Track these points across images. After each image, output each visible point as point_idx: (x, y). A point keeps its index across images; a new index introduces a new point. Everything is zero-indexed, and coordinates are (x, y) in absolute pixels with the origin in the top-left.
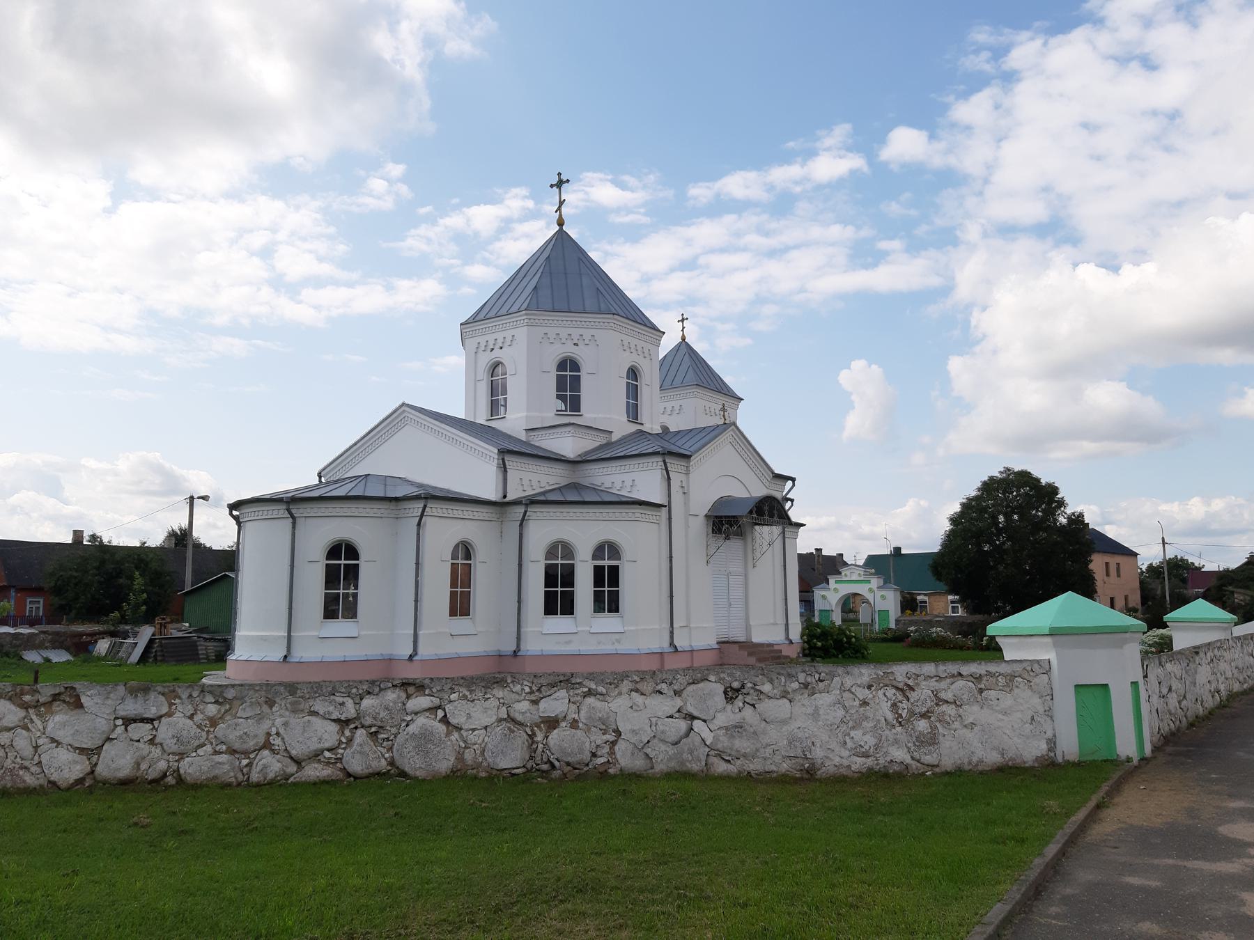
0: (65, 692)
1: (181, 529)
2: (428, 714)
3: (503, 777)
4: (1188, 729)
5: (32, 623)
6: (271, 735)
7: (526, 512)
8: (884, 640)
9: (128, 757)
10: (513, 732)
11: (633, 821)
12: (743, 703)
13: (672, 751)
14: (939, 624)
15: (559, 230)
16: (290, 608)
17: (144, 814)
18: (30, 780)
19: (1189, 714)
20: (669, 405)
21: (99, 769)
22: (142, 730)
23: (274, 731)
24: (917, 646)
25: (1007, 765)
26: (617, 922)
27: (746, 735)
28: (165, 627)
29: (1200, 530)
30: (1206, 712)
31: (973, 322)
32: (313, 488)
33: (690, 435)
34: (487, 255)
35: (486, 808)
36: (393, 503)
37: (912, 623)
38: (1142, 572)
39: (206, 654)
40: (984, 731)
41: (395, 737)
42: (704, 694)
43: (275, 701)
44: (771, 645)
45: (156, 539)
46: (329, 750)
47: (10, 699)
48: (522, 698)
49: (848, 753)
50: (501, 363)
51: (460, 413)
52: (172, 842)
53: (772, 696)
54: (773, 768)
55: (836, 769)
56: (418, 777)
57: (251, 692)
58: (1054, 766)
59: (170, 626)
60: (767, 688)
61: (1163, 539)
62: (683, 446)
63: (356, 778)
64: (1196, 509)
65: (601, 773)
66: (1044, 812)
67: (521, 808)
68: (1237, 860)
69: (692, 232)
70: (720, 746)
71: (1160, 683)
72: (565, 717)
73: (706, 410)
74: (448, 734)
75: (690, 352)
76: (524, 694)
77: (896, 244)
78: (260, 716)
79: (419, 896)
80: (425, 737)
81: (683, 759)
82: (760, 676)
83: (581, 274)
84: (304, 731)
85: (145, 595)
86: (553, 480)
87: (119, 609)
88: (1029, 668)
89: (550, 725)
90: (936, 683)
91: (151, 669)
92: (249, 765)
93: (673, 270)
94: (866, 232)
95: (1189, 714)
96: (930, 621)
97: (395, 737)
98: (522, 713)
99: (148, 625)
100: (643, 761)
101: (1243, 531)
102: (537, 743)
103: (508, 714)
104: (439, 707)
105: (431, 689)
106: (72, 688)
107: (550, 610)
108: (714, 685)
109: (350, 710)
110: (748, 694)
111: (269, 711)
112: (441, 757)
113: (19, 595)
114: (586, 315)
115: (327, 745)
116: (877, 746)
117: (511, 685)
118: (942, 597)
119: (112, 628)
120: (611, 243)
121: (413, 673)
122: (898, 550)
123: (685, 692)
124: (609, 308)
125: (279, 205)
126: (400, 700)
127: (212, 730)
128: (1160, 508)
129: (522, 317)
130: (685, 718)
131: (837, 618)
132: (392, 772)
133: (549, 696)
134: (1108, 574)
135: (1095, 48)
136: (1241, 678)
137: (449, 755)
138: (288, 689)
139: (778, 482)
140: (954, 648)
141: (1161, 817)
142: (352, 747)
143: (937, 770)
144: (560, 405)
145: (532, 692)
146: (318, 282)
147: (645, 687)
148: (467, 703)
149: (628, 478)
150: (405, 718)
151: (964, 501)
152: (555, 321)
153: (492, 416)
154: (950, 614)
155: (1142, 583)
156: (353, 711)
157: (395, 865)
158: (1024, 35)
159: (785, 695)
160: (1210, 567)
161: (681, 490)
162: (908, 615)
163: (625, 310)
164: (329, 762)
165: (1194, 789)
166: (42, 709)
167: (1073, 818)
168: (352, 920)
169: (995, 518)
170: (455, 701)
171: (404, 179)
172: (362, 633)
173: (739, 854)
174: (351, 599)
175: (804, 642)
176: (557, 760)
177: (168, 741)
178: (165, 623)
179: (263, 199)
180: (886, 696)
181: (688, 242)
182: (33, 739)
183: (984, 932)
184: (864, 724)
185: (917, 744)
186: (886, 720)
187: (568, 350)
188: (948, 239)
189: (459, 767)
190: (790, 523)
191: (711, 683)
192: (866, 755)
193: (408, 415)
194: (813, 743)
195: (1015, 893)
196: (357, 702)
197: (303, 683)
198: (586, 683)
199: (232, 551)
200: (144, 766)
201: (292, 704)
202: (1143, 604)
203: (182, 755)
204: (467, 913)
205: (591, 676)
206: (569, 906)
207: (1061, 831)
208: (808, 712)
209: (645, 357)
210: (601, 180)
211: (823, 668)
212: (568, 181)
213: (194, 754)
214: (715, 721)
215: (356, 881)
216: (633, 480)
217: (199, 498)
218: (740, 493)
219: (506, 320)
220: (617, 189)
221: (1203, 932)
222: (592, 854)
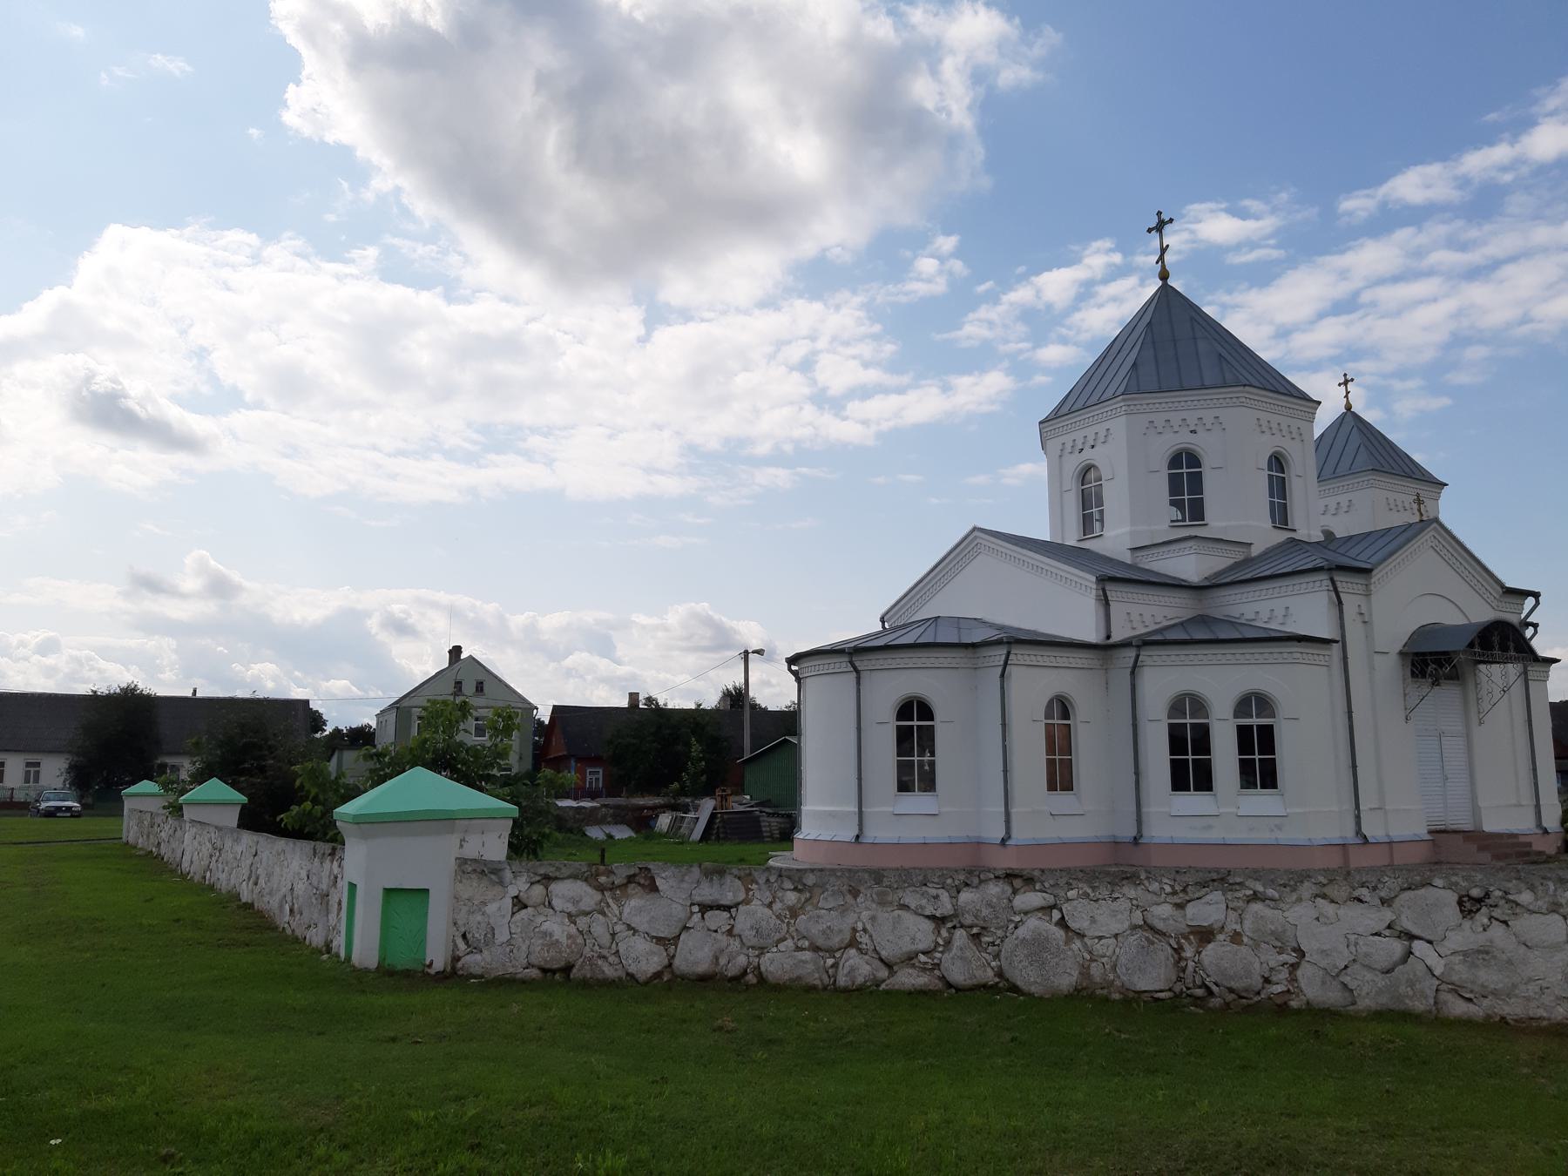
0: (640, 873)
1: (735, 688)
2: (1040, 915)
5: (593, 795)
6: (857, 931)
7: (1138, 657)
9: (706, 950)
10: (1153, 943)
12: (1490, 919)
16: (860, 779)
17: (728, 1016)
18: (609, 972)
20: (1332, 502)
21: (677, 962)
22: (718, 919)
23: (860, 926)
28: (726, 800)
32: (876, 635)
33: (1386, 539)
34: (1064, 331)
36: (970, 650)
39: (770, 832)
41: (1002, 941)
42: (1427, 905)
43: (859, 891)
45: (711, 700)
46: (923, 953)
47: (586, 880)
48: (1162, 900)
50: (1093, 466)
51: (1044, 535)
52: (760, 1053)
53: (1536, 909)
54: (1542, 1013)
57: (832, 879)
59: (731, 799)
60: (1525, 897)
63: (958, 990)
65: (1279, 1006)
69: (1348, 259)
70: (1455, 978)
74: (1068, 942)
75: (1361, 426)
76: (1164, 895)
78: (843, 908)
79: (1055, 1148)
80: (1038, 945)
82: (1514, 881)
83: (1195, 338)
84: (894, 928)
85: (703, 763)
86: (1171, 613)
87: (679, 779)
91: (715, 849)
92: (835, 966)
93: (1321, 316)
97: (1002, 941)
98: (1163, 919)
99: (708, 798)
100: (1340, 994)
102: (1186, 960)
105: (1042, 882)
106: (647, 869)
108: (1442, 892)
109: (945, 906)
110: (1496, 906)
111: (853, 902)
113: (579, 765)
114: (1184, 393)
115: (921, 946)
117: (1146, 882)
119: (673, 801)
120: (1230, 292)
125: (817, 306)
126: (1004, 896)
127: (793, 921)
129: (1118, 404)
130: (1399, 937)
132: (1001, 985)
133: (1198, 899)
138: (873, 876)
139: (1515, 599)
142: (950, 950)
144: (1175, 513)
145: (1174, 893)
147: (1336, 892)
152: (1189, 402)
153: (1084, 535)
156: (949, 906)
163: (1262, 380)
166: (618, 892)
168: (977, 1168)
171: (958, 253)
174: (927, 768)
177: (747, 933)
178: (726, 795)
179: (800, 304)
181: (1343, 274)
182: (610, 925)
187: (1183, 440)
189: (1084, 984)
193: (981, 541)
196: (953, 895)
198: (1249, 883)
199: (790, 711)
200: (723, 961)
203: (762, 950)
205: (1256, 875)
210: (1212, 211)
212: (1171, 220)
213: (775, 949)
214: (1446, 943)
217: (753, 652)
218: (1452, 618)
219: (1097, 410)
220: (1235, 219)
222: (1282, 1114)
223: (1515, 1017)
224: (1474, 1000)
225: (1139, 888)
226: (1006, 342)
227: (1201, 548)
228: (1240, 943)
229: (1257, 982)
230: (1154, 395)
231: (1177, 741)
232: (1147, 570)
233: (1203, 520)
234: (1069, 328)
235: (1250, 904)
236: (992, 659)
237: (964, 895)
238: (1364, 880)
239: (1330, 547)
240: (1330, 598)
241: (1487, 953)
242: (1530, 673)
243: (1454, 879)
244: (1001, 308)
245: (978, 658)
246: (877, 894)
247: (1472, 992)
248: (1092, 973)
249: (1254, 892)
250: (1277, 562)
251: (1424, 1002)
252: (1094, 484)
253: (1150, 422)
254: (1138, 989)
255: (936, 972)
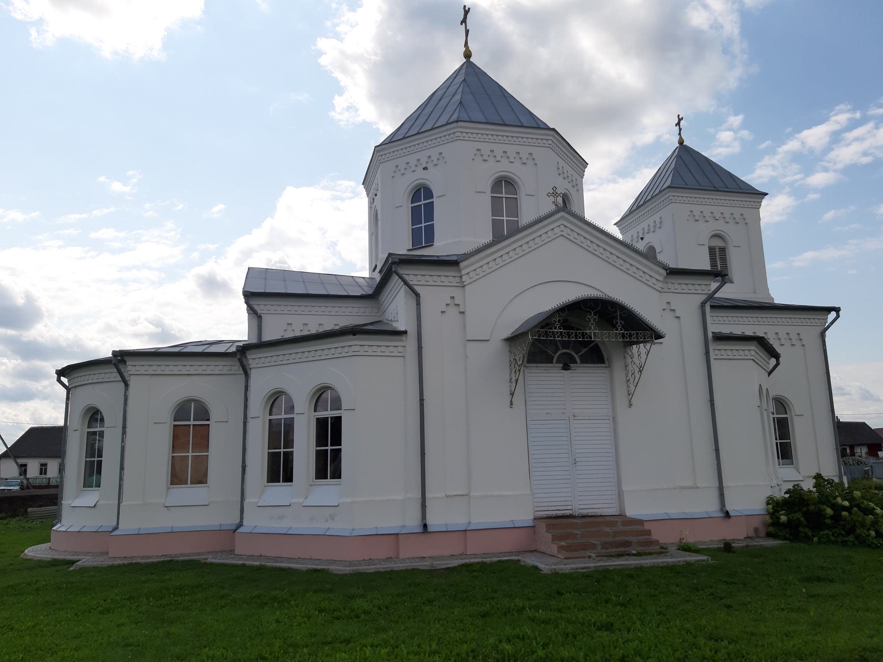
107: (321, 474)
226: (785, 176)
234: (829, 162)
244: (778, 157)
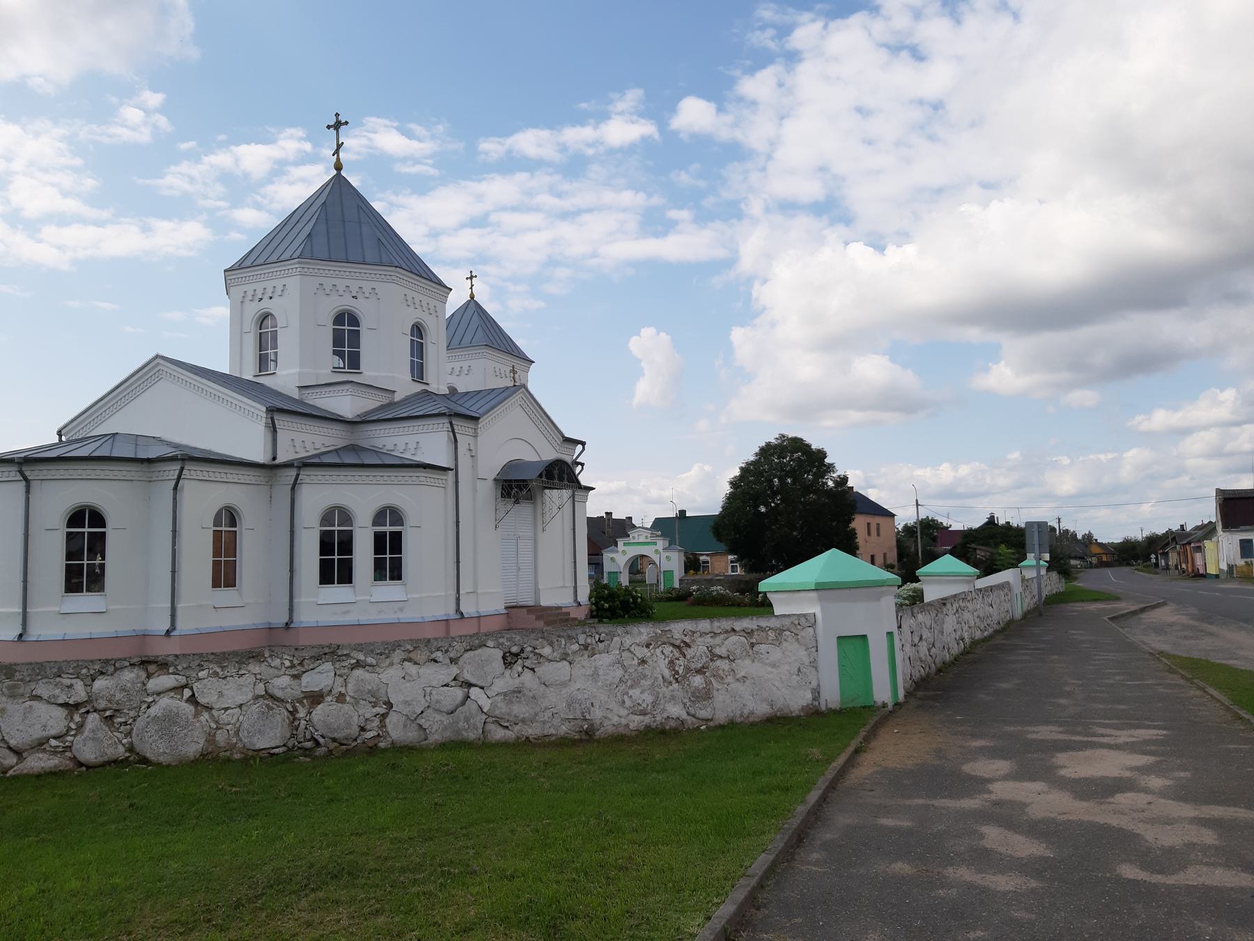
2: (172, 694)
3: (260, 758)
4: (936, 674)
7: (298, 475)
8: (669, 599)
10: (272, 709)
11: (401, 796)
12: (523, 668)
13: (446, 720)
14: (719, 582)
15: (337, 174)
16: (25, 581)
19: (938, 660)
20: (457, 366)
24: (699, 604)
25: (776, 715)
26: (372, 908)
27: (525, 700)
29: (947, 493)
30: (952, 658)
31: (755, 294)
32: (51, 447)
33: (491, 396)
35: (236, 793)
36: (145, 466)
37: (694, 582)
38: (899, 532)
40: (754, 684)
42: (482, 661)
44: (560, 608)
46: (55, 738)
48: (282, 673)
49: (626, 712)
50: (271, 315)
51: (226, 370)
54: (552, 731)
55: (615, 728)
56: (162, 763)
58: (818, 714)
60: (547, 651)
61: (917, 500)
62: (471, 408)
63: (88, 767)
64: (945, 474)
65: (371, 748)
66: (808, 759)
67: (277, 791)
68: (978, 796)
69: (482, 187)
70: (497, 713)
71: (912, 633)
72: (331, 691)
73: (495, 372)
74: (197, 715)
75: (479, 311)
76: (284, 669)
77: (684, 214)
80: (170, 719)
81: (459, 729)
82: (540, 640)
84: (25, 718)
86: (328, 441)
88: (796, 622)
89: (313, 700)
90: (710, 640)
93: (463, 226)
94: (656, 201)
95: (938, 660)
96: (711, 580)
97: (134, 720)
98: (282, 689)
100: (416, 733)
101: (985, 494)
103: (265, 690)
104: (185, 686)
105: (176, 666)
107: (326, 577)
108: (492, 650)
109: (79, 692)
110: (527, 658)
112: (188, 740)
115: (53, 732)
116: (654, 704)
117: (269, 659)
118: (723, 557)
120: (396, 193)
121: (163, 650)
122: (683, 512)
123: (461, 659)
124: (391, 260)
125: (14, 130)
126: (139, 680)
128: (915, 473)
130: (461, 686)
131: (624, 580)
132: (131, 759)
133: (312, 669)
134: (869, 534)
135: (870, 35)
136: (982, 627)
137: (197, 737)
140: (733, 605)
141: (912, 759)
142: (82, 733)
143: (711, 724)
144: (337, 362)
145: (293, 666)
146: (62, 220)
147: (419, 656)
148: (218, 681)
149: (412, 440)
150: (146, 699)
151: (743, 465)
153: (260, 372)
154: (730, 573)
155: (898, 541)
156: (83, 694)
157: (125, 863)
158: (807, 16)
159: (564, 657)
160: (956, 526)
161: (468, 454)
162: (692, 575)
164: (56, 752)
165: (941, 731)
167: (834, 764)
168: (64, 930)
169: (770, 481)
170: (204, 679)
171: (162, 110)
172: (110, 607)
173: (510, 823)
175: (592, 604)
176: (323, 736)
180: (663, 654)
181: (479, 198)
183: (749, 885)
184: (643, 682)
185: (692, 699)
186: (663, 677)
187: (346, 303)
188: (733, 212)
189: (210, 749)
190: (580, 487)
191: (488, 649)
192: (644, 713)
194: (592, 704)
195: (777, 842)
196: (88, 683)
197: (23, 664)
201: (8, 688)
202: (899, 561)
204: (203, 912)
205: (359, 648)
206: (321, 894)
207: (822, 777)
208: (587, 673)
209: (431, 314)
210: (386, 126)
211: (604, 629)
212: (346, 123)
214: (492, 687)
215: (75, 884)
216: (418, 443)
218: (531, 457)
221: (948, 868)
222: (352, 834)
223: (535, 736)
224: (510, 727)
225: (263, 665)
227: (356, 391)
228: (344, 702)
229: (355, 731)
230: (324, 262)
231: (326, 545)
232: (310, 405)
233: (359, 369)
234: (264, 197)
235: (353, 671)
236: (167, 473)
237: (99, 682)
238: (439, 646)
239: (452, 399)
240: (449, 437)
241: (520, 692)
242: (576, 497)
243: (501, 640)
245: (153, 472)
246: (8, 688)
247: (508, 721)
248: (217, 739)
249: (357, 661)
250: (421, 404)
251: (475, 732)
252: (270, 330)
253: (360, 287)
254: (257, 748)
255: (67, 754)
